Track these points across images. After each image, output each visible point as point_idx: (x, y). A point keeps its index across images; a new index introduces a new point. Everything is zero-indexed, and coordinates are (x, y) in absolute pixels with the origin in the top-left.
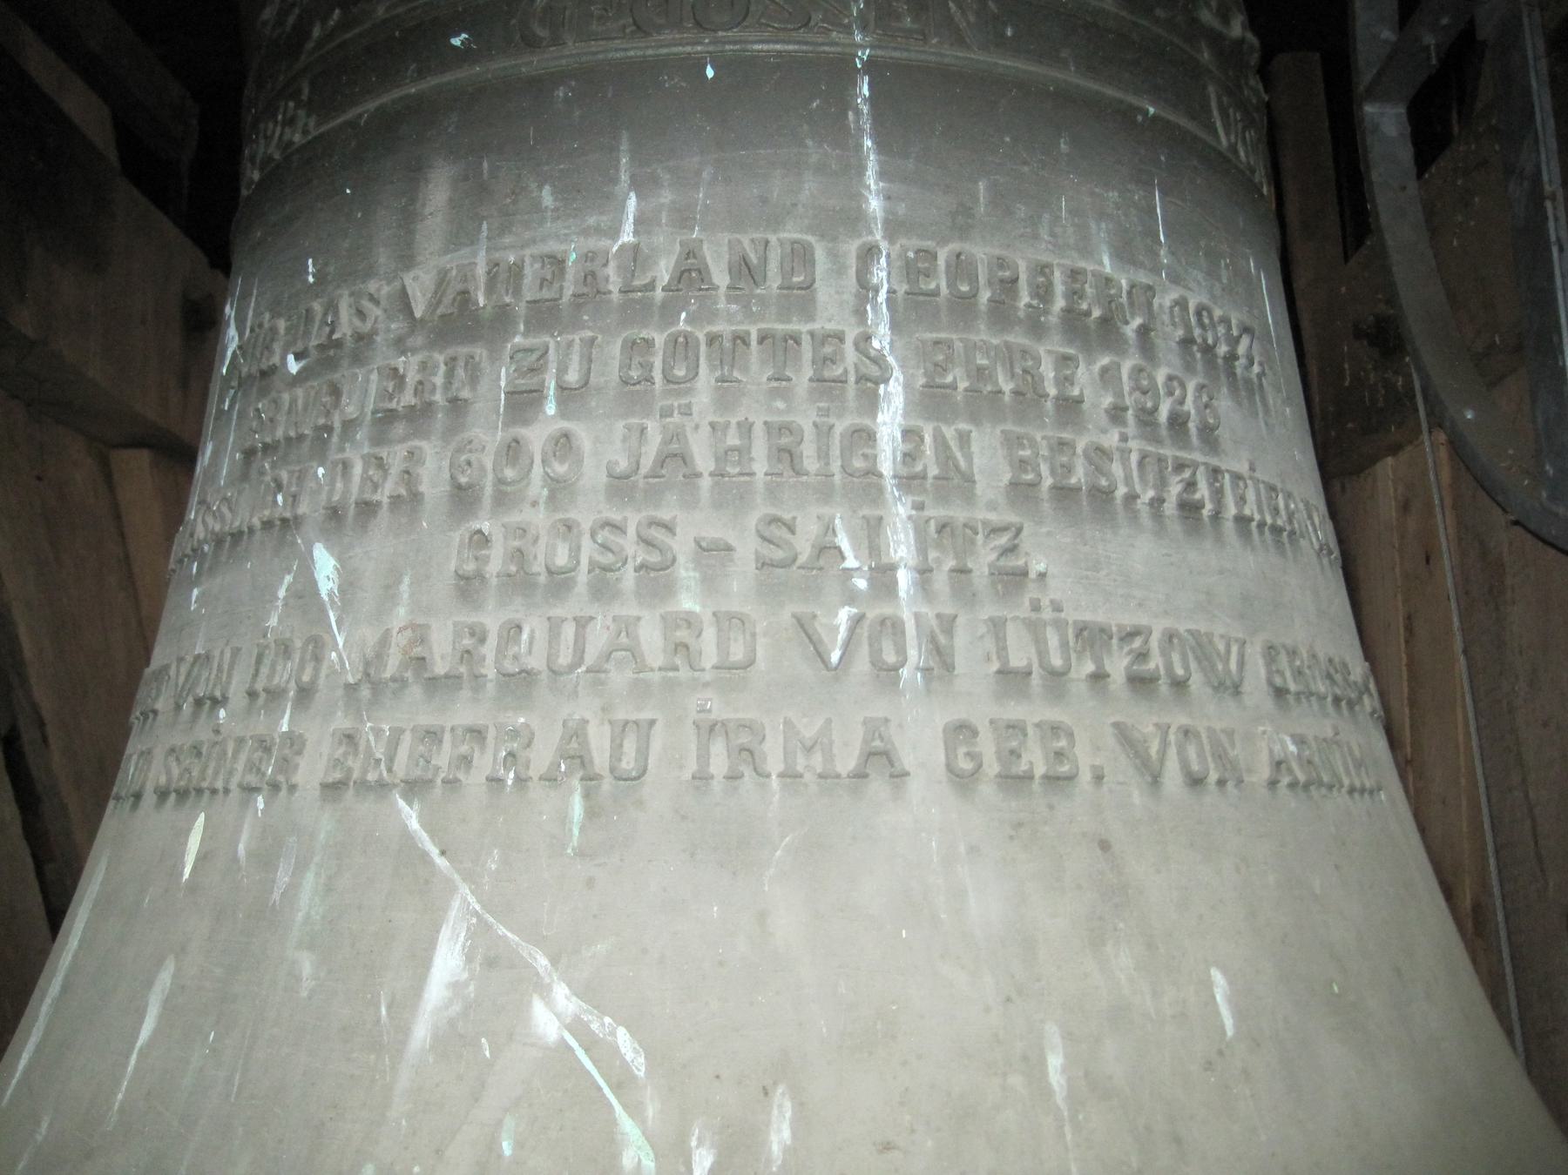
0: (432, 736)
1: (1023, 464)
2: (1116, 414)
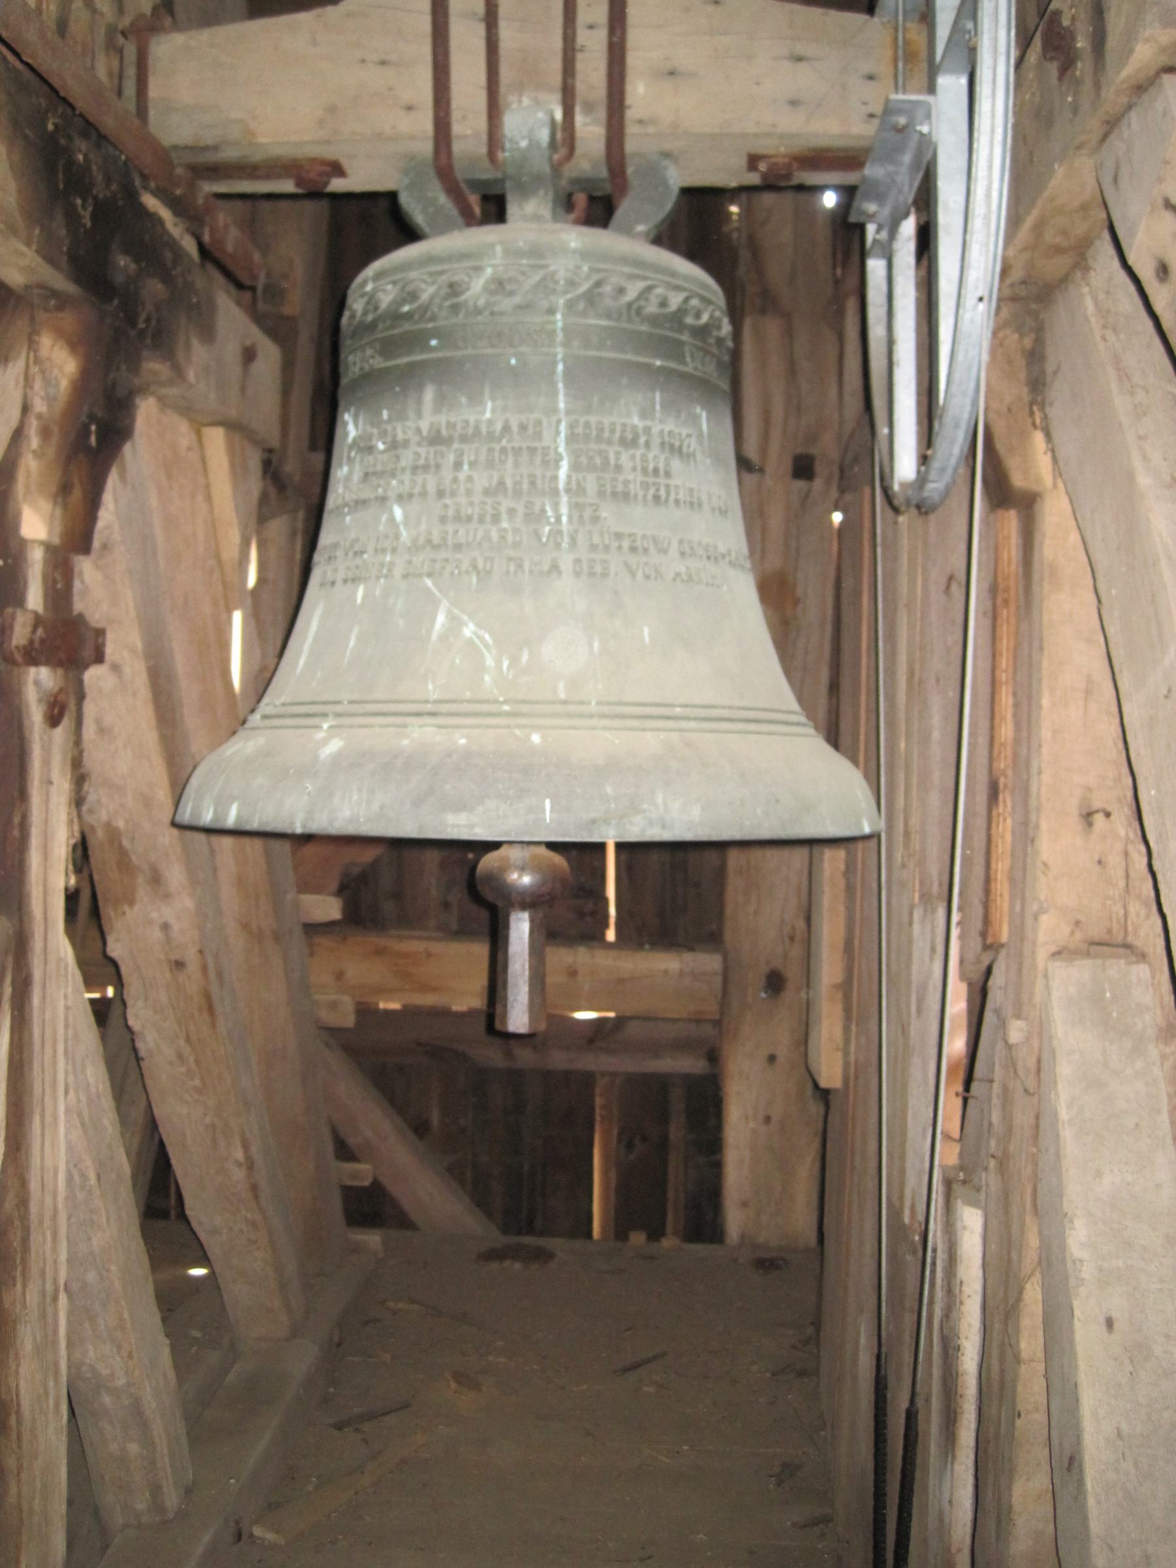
0: (434, 561)
1: (603, 486)
2: (634, 469)
